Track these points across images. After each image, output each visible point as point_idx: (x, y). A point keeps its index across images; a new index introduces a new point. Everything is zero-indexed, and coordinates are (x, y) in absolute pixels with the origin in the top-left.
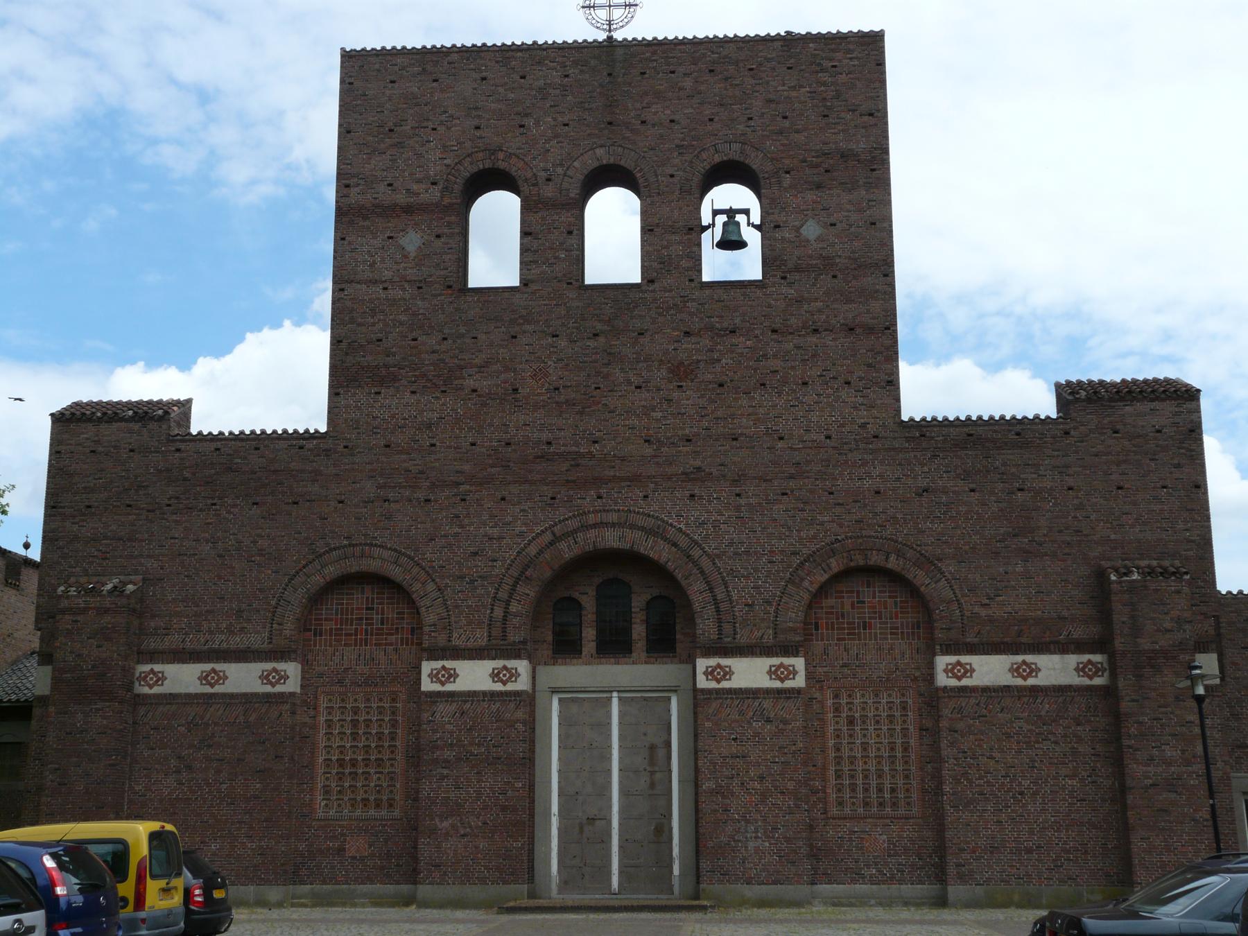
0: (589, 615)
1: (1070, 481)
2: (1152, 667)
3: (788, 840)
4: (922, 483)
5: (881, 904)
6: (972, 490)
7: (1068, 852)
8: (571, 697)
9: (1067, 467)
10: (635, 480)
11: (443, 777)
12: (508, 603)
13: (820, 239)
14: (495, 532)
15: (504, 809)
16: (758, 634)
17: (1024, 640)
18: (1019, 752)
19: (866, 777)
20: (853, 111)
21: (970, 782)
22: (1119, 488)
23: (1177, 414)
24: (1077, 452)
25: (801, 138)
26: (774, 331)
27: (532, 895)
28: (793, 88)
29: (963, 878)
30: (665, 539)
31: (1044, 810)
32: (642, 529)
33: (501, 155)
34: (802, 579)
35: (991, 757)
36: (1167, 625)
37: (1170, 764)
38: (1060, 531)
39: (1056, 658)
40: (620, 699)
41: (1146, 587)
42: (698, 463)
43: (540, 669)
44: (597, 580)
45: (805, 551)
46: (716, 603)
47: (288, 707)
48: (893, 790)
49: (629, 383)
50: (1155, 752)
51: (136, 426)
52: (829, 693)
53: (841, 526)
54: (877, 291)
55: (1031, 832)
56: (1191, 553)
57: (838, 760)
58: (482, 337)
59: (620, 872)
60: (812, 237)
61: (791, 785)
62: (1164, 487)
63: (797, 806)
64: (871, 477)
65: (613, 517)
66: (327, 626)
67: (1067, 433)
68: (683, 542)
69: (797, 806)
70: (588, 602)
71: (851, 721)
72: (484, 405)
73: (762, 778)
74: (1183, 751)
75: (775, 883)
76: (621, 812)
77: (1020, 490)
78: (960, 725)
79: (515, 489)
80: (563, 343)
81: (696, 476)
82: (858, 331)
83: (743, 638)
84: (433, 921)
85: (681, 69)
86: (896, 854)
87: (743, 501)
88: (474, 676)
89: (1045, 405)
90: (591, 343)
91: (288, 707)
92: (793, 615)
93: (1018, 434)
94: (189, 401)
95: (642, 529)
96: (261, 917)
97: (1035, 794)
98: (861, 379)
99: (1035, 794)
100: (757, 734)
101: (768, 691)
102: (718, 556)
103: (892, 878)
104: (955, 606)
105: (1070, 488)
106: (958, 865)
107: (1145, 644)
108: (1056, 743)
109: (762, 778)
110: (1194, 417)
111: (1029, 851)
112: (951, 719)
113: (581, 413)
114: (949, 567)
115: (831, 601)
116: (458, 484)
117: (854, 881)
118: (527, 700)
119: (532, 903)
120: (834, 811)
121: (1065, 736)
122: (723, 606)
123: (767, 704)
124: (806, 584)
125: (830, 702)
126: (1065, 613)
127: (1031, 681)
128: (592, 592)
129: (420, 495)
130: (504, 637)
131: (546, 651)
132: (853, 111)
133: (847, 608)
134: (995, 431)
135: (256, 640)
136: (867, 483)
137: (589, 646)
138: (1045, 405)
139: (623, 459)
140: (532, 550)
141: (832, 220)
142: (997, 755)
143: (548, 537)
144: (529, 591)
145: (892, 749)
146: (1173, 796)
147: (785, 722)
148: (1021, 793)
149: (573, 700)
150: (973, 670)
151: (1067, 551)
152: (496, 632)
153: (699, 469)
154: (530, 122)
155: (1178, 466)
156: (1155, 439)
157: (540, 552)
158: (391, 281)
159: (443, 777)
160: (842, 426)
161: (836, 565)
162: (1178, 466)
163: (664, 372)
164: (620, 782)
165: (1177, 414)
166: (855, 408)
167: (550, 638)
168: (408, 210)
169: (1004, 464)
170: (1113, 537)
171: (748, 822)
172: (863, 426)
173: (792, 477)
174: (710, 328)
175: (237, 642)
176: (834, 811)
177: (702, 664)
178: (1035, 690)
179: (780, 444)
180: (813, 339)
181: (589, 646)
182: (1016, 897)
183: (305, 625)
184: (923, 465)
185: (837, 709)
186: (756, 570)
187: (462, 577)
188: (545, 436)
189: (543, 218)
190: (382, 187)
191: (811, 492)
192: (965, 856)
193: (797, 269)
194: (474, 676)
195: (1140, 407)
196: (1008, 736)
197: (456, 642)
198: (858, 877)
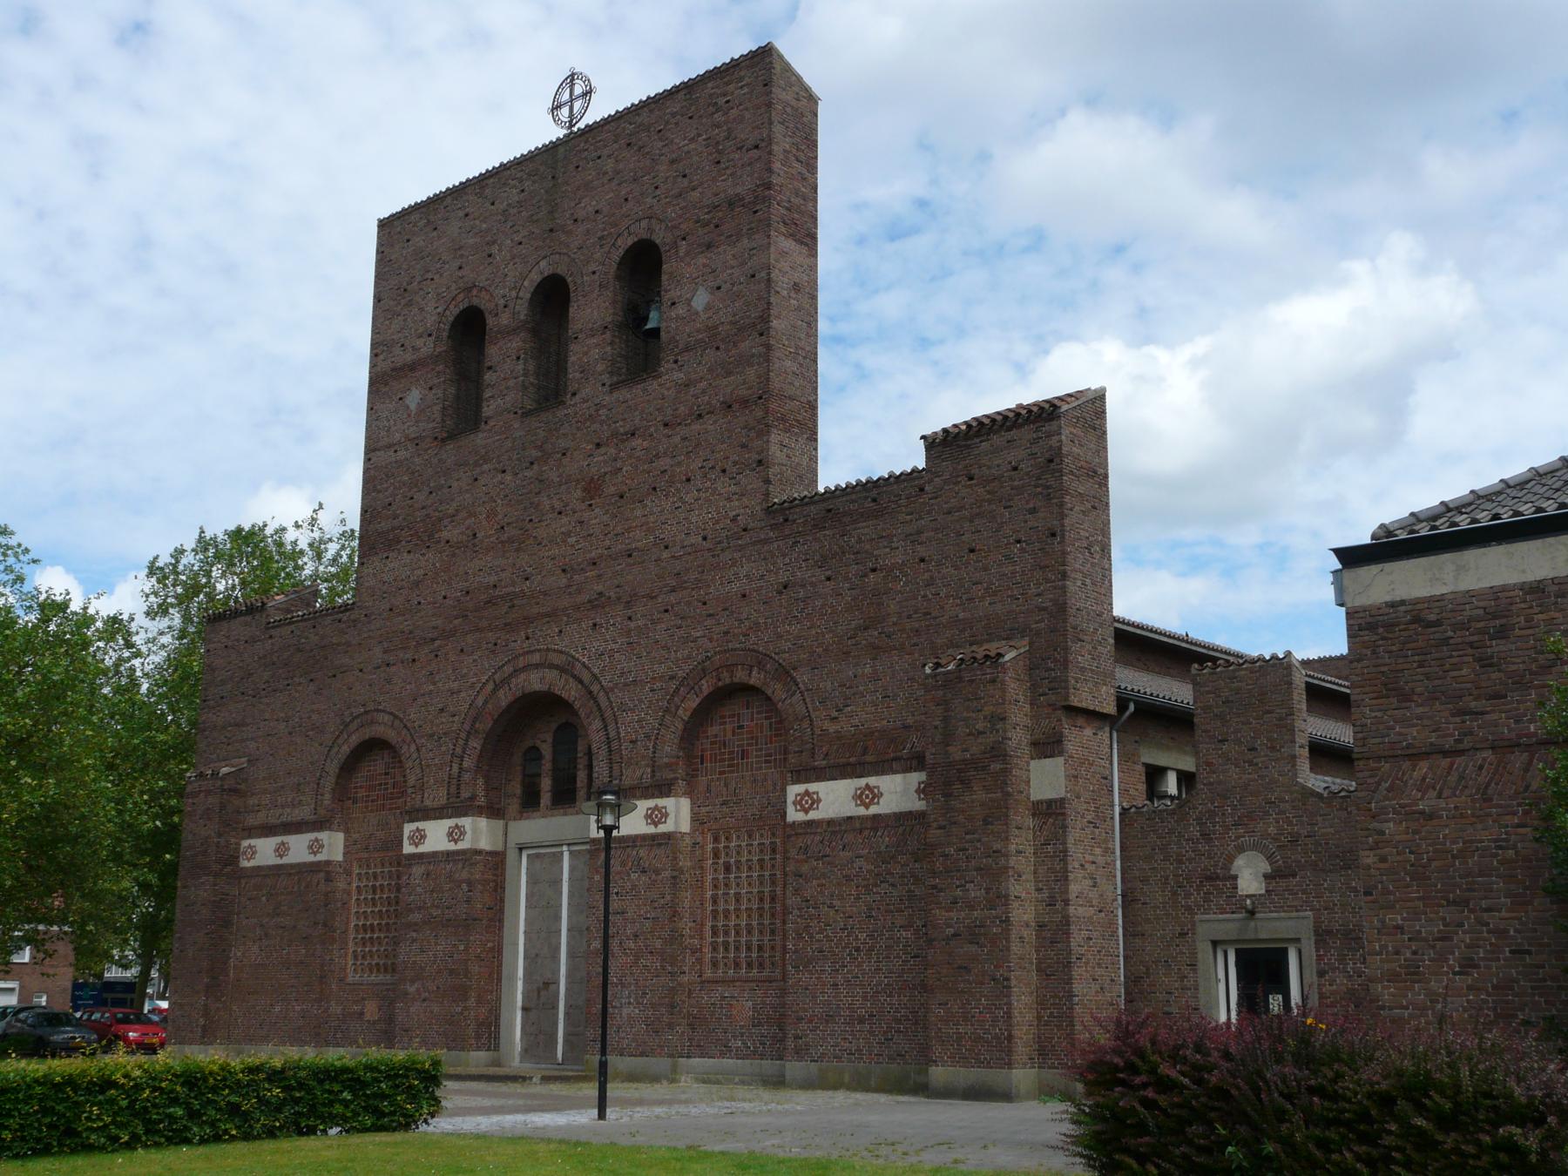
0: (547, 765)
1: (922, 551)
2: (962, 782)
3: (653, 1006)
4: (783, 577)
5: (743, 1083)
6: (829, 579)
7: (898, 1021)
8: (545, 857)
9: (919, 532)
10: (552, 615)
11: (414, 940)
12: (462, 758)
13: (708, 307)
14: (455, 685)
15: (452, 972)
16: (638, 773)
17: (869, 758)
18: (858, 898)
19: (737, 933)
20: (740, 148)
21: (811, 937)
22: (972, 551)
23: (1035, 441)
24: (929, 512)
25: (696, 194)
26: (666, 425)
27: (497, 1063)
28: (692, 140)
29: (799, 1053)
30: (574, 677)
31: (878, 969)
32: (557, 667)
33: (474, 292)
34: (678, 708)
35: (831, 906)
36: (980, 726)
37: (972, 908)
38: (909, 617)
39: (898, 778)
40: (571, 853)
41: (960, 679)
42: (600, 588)
44: (554, 726)
45: (681, 674)
47: (322, 875)
48: (760, 948)
49: (553, 508)
50: (959, 892)
51: (248, 618)
52: (709, 837)
53: (711, 640)
54: (753, 356)
55: (865, 998)
56: (1042, 625)
57: (715, 913)
58: (455, 484)
59: (565, 1041)
61: (658, 944)
62: (1019, 542)
63: (663, 968)
64: (738, 579)
65: (536, 658)
66: (362, 793)
67: (922, 490)
68: (586, 677)
69: (663, 968)
70: (546, 750)
71: (727, 869)
72: (454, 555)
74: (988, 890)
75: (642, 1054)
76: (568, 976)
77: (874, 570)
78: (805, 868)
79: (470, 639)
80: (508, 477)
81: (598, 603)
82: (736, 406)
84: (640, 1102)
85: (606, 152)
86: (760, 1024)
87: (632, 625)
88: (436, 836)
89: (917, 459)
90: (528, 473)
91: (322, 875)
92: (669, 748)
93: (874, 500)
95: (557, 667)
97: (871, 949)
98: (735, 463)
99: (871, 949)
100: (634, 887)
101: (644, 837)
102: (612, 690)
103: (754, 1053)
104: (806, 724)
105: (922, 560)
106: (797, 1037)
107: (956, 753)
108: (893, 885)
111: (861, 1021)
112: (797, 861)
113: (518, 550)
114: (803, 677)
115: (713, 730)
116: (433, 640)
117: (722, 1055)
118: (496, 862)
119: (492, 1071)
121: (903, 876)
122: (615, 745)
124: (680, 712)
125: (710, 847)
126: (910, 721)
127: (873, 810)
128: (549, 738)
129: (409, 656)
130: (458, 795)
131: (514, 806)
132: (740, 148)
133: (729, 735)
134: (853, 501)
135: (304, 813)
136: (735, 587)
137: (546, 799)
138: (917, 459)
139: (545, 594)
140: (480, 702)
142: (836, 903)
143: (490, 686)
144: (476, 744)
145: (761, 900)
146: (974, 948)
147: (657, 872)
148: (858, 949)
149: (538, 856)
150: (819, 800)
151: (915, 640)
153: (600, 594)
154: (495, 249)
155: (1033, 511)
156: (1011, 479)
157: (486, 702)
158: (400, 443)
159: (414, 940)
160: (717, 522)
161: (706, 687)
162: (1033, 511)
163: (579, 492)
164: (568, 943)
165: (1035, 441)
166: (729, 499)
167: (519, 791)
169: (860, 541)
170: (961, 616)
171: (623, 985)
172: (734, 520)
173: (673, 590)
174: (615, 434)
176: (708, 974)
179: (665, 555)
180: (696, 427)
181: (546, 799)
182: (847, 1078)
183: (342, 792)
184: (784, 555)
185: (716, 855)
186: (640, 701)
187: (432, 736)
188: (493, 579)
189: (501, 349)
190: (398, 350)
191: (689, 604)
192: (803, 1025)
193: (687, 349)
194: (436, 836)
195: (997, 440)
197: (428, 803)
198: (725, 1051)
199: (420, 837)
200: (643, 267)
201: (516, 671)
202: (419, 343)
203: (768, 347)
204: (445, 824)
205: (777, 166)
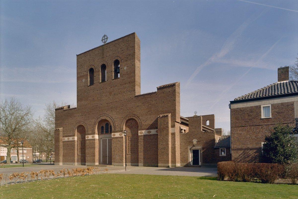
43: (100, 136)
46: (114, 125)
60: (125, 69)
73: (118, 149)
75: (120, 163)
80: (98, 91)
83: (117, 130)
89: (156, 90)
94: (230, 101)
96: (47, 166)
109: (118, 149)
110: (175, 88)
120: (128, 153)
122: (115, 126)
123: (119, 139)
127: (150, 134)
137: (104, 133)
138: (156, 90)
141: (128, 66)
152: (92, 131)
162: (172, 97)
168: (83, 76)
175: (70, 134)
177: (112, 134)
178: (151, 135)
180: (125, 85)
196: (147, 142)
199: (88, 137)
200: (117, 63)
201: (100, 117)
202: (84, 73)
203: (135, 75)
204: (119, 133)
205: (136, 50)
